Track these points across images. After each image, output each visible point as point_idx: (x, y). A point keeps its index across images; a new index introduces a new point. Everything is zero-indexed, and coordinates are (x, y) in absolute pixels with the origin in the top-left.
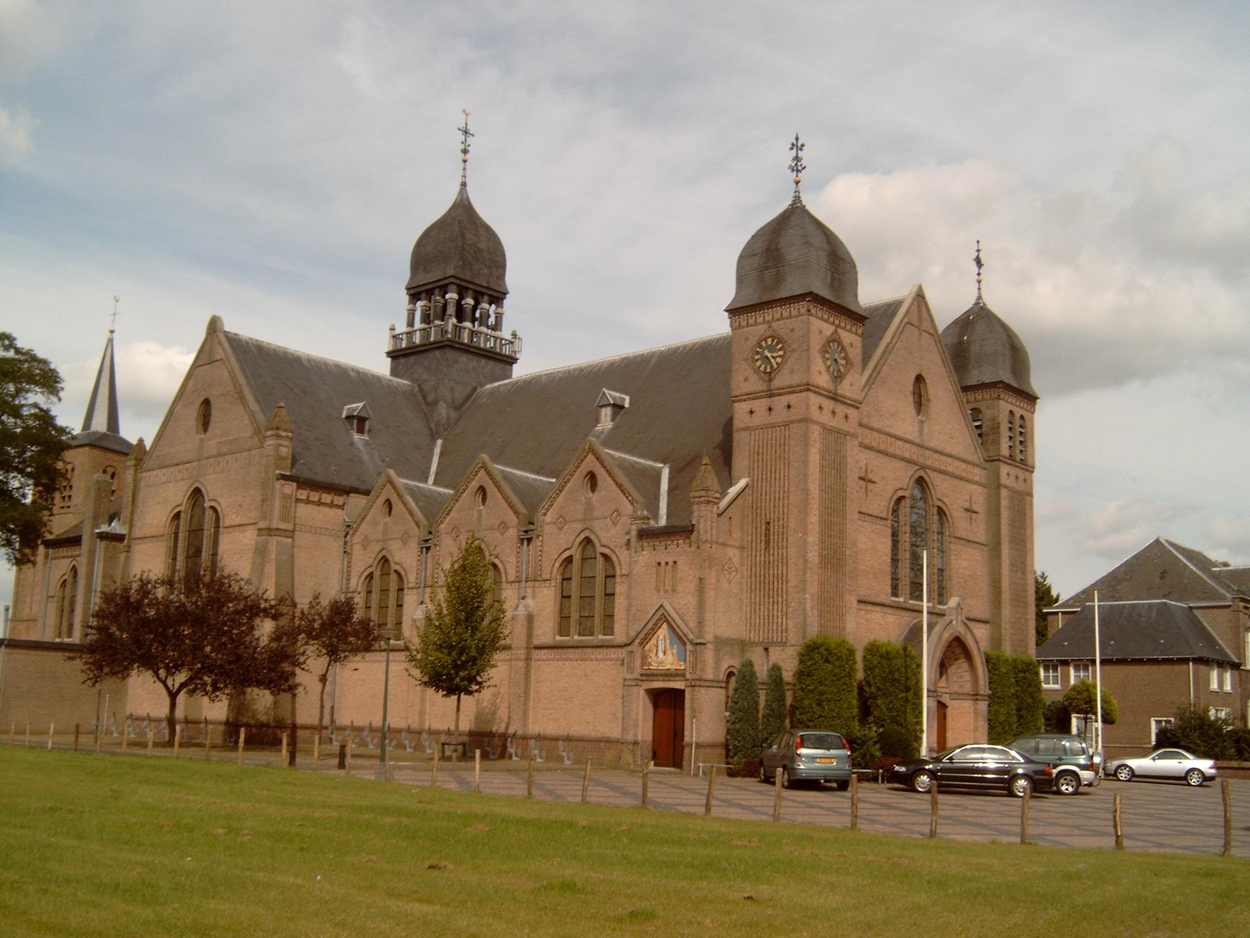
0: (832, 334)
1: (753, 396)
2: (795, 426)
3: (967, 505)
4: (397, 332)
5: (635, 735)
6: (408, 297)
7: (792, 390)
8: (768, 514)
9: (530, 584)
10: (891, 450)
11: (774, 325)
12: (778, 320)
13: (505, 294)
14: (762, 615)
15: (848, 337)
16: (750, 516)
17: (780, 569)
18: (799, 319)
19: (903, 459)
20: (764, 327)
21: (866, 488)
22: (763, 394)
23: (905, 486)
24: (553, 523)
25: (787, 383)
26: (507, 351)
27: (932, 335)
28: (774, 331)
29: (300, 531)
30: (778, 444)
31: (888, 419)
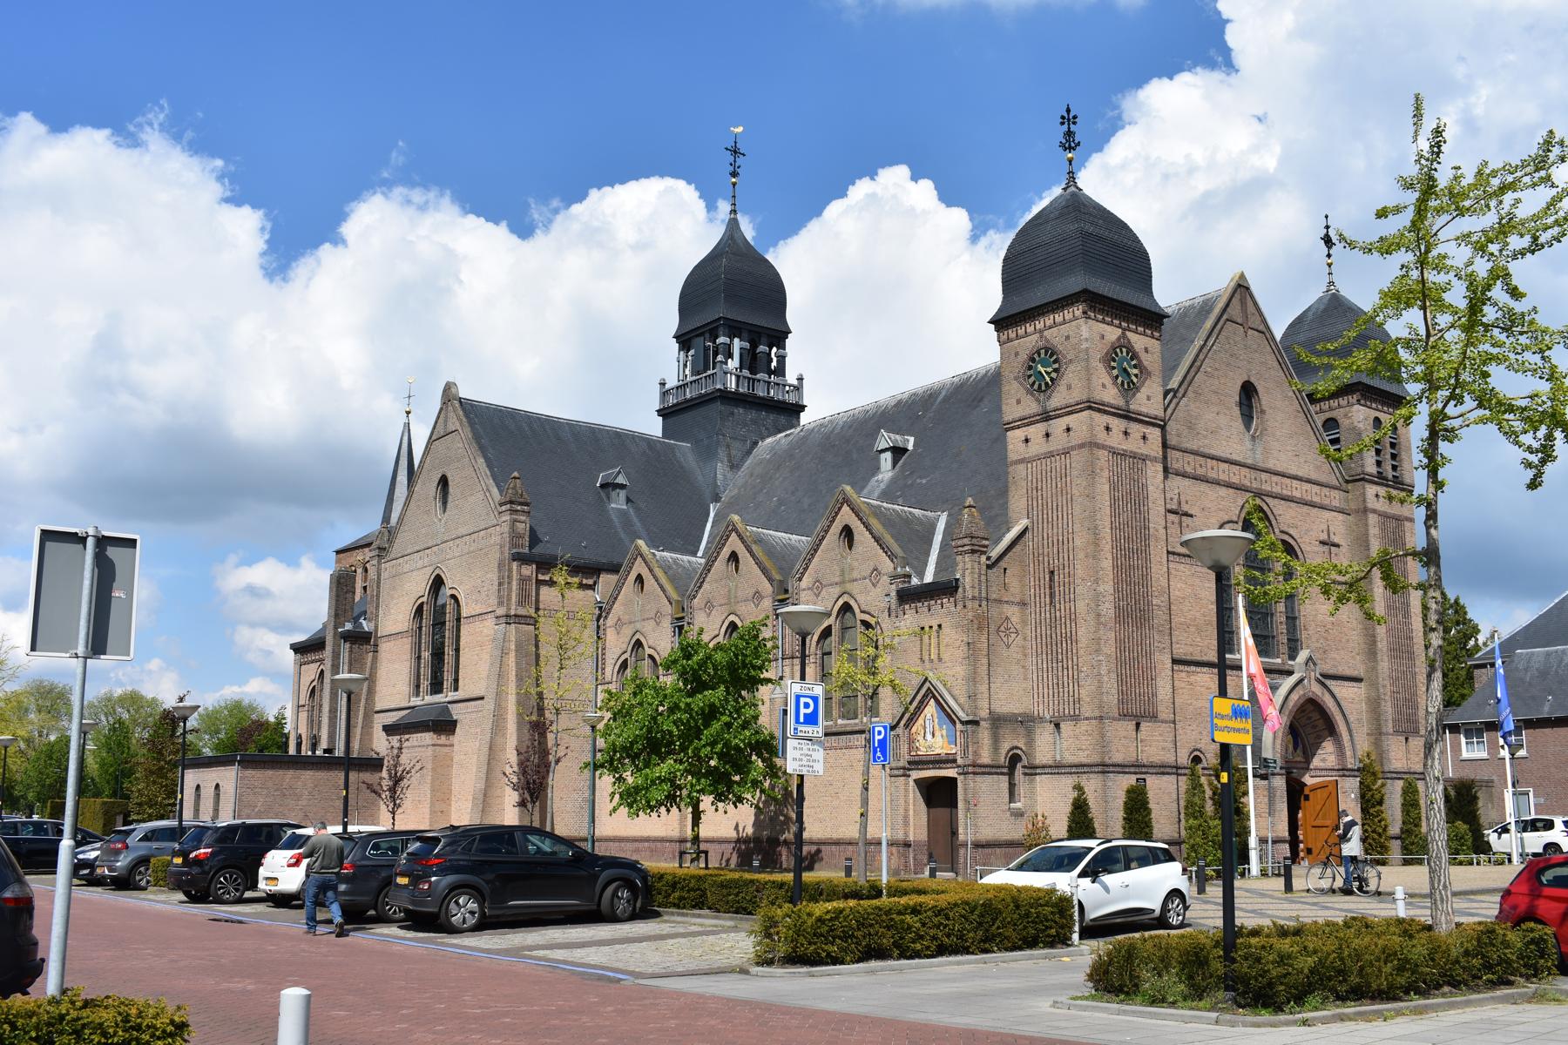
0: (1119, 339)
1: (1026, 421)
2: (1075, 453)
3: (1324, 537)
5: (906, 834)
7: (1070, 410)
8: (1051, 562)
9: (787, 662)
10: (1212, 475)
13: (787, 332)
14: (1050, 683)
15: (1139, 341)
16: (1032, 565)
17: (1068, 626)
18: (1073, 323)
19: (1229, 485)
20: (1036, 337)
21: (1180, 523)
22: (1038, 418)
23: (1235, 519)
24: (809, 589)
25: (1063, 403)
26: (791, 398)
27: (1263, 333)
28: (1047, 340)
29: (545, 616)
30: (1059, 475)
31: (1205, 437)
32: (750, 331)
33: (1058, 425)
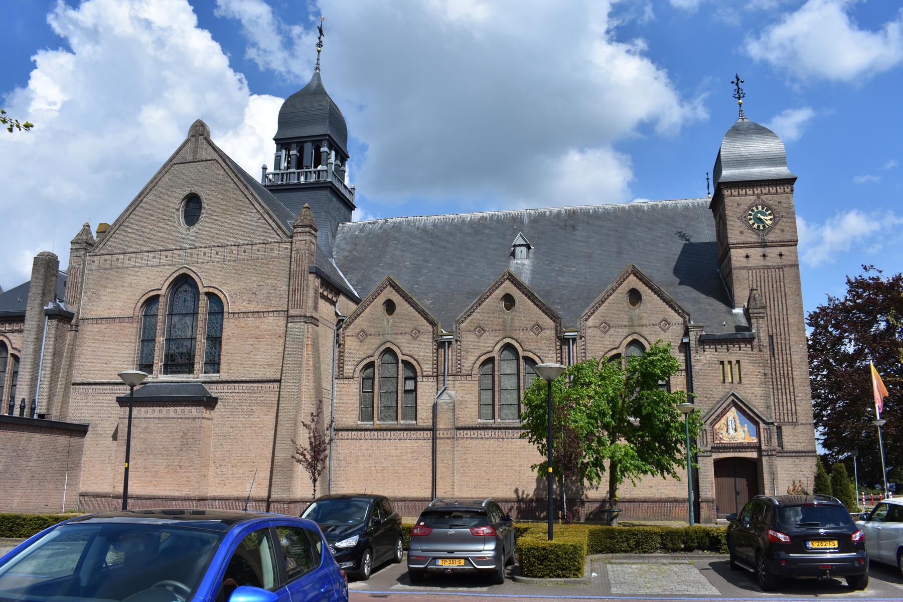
4: (268, 171)
6: (276, 145)
8: (770, 330)
11: (762, 197)
12: (766, 194)
20: (755, 197)
22: (757, 244)
25: (779, 239)
30: (774, 280)
32: (297, 143)
33: (773, 252)
